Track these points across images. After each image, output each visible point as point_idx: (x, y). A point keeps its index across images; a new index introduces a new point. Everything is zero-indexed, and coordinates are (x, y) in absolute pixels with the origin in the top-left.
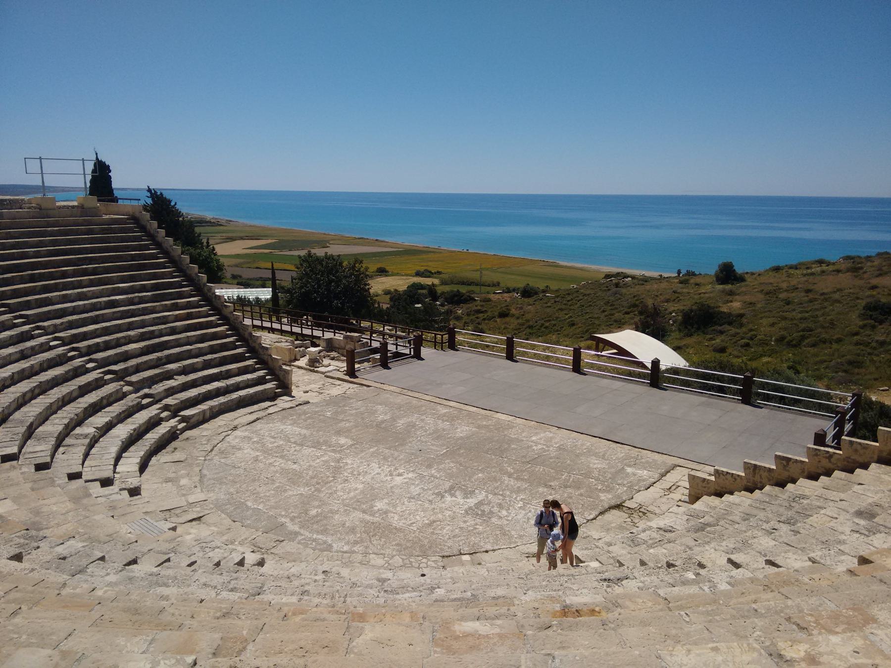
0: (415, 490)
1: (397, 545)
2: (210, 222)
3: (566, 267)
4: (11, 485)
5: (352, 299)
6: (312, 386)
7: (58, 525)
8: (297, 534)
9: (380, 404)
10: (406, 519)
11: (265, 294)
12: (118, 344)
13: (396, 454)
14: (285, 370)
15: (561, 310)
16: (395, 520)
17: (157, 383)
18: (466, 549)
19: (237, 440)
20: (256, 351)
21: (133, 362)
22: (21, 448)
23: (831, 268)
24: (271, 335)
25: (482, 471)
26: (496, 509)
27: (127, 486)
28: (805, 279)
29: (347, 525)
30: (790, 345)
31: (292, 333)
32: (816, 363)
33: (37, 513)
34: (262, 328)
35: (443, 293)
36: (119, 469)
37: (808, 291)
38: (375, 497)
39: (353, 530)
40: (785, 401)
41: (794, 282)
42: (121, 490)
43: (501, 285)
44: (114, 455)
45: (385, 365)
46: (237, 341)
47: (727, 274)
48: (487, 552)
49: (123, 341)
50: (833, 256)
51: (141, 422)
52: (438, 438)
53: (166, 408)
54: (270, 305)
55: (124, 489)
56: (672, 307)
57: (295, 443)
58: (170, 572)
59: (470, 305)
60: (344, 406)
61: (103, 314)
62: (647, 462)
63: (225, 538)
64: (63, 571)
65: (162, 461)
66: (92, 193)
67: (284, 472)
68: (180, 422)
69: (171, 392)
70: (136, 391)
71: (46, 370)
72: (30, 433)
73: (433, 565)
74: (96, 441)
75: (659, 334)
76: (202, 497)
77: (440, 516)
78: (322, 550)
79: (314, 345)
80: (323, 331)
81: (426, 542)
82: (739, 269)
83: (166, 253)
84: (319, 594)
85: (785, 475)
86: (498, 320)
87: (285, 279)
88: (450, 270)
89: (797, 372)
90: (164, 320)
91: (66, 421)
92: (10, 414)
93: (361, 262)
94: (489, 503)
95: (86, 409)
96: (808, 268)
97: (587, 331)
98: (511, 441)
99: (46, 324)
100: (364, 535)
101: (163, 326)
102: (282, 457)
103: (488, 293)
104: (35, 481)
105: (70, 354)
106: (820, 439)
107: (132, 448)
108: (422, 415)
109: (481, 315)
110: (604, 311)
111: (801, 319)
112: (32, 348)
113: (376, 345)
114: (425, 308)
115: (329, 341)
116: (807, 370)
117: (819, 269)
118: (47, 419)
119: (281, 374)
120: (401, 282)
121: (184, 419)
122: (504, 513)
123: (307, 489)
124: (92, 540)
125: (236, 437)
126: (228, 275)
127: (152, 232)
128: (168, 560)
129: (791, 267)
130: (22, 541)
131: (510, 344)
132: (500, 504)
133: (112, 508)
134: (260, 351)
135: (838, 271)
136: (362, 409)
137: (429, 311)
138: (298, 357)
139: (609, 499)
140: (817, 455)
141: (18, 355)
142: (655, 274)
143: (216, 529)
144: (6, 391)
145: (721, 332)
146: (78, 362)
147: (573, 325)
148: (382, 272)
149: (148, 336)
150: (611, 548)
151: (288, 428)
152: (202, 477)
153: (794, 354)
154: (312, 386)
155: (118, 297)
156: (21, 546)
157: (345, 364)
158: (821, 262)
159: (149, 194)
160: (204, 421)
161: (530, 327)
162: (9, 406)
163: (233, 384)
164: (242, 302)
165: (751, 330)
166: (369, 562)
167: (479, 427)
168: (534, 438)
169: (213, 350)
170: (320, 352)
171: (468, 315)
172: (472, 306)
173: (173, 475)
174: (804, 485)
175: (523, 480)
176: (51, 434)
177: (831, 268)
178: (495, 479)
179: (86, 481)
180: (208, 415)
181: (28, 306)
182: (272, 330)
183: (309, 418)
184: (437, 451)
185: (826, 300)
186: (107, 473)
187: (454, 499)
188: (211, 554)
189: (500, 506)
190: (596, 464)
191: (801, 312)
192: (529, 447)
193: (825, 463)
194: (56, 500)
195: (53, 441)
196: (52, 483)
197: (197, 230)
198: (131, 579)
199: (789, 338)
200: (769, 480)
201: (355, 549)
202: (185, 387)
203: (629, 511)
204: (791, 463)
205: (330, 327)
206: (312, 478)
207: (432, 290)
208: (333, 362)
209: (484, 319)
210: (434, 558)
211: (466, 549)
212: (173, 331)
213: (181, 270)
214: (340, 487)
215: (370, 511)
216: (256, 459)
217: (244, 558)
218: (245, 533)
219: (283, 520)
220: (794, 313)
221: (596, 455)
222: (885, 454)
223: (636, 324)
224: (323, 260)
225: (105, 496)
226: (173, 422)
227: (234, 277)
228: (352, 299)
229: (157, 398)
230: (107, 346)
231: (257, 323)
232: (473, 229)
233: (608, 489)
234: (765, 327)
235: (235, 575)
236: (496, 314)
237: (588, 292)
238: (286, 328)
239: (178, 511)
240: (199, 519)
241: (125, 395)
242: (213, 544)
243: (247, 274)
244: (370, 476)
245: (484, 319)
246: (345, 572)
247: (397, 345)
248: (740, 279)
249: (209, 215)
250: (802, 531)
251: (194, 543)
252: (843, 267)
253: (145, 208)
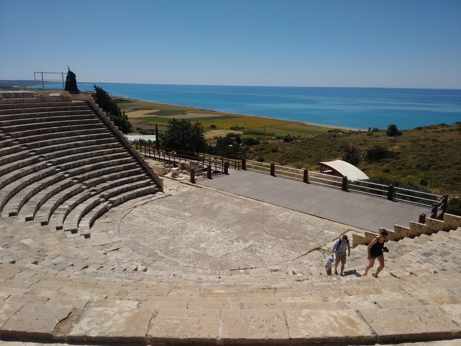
0: (220, 239)
1: (209, 264)
2: (126, 101)
3: (310, 126)
4: (31, 232)
5: (195, 143)
6: (173, 187)
7: (52, 250)
8: (163, 257)
9: (206, 197)
10: (215, 252)
11: (153, 138)
12: (80, 165)
13: (212, 221)
14: (161, 180)
15: (305, 149)
16: (209, 252)
17: (98, 184)
18: (242, 267)
19: (136, 213)
20: (146, 169)
21: (87, 174)
22: (35, 214)
23: (448, 128)
24: (154, 161)
25: (253, 230)
26: (258, 249)
27: (84, 234)
28: (433, 134)
29: (187, 254)
30: (423, 169)
31: (164, 160)
32: (436, 179)
33: (43, 245)
34: (150, 157)
35: (244, 139)
36: (80, 225)
37: (435, 141)
38: (200, 242)
39: (189, 257)
40: (413, 199)
41: (428, 136)
42: (81, 235)
43: (276, 135)
44: (78, 219)
45: (210, 177)
46: (137, 164)
47: (393, 131)
48: (252, 268)
49: (82, 163)
50: (450, 122)
51: (91, 203)
52: (233, 214)
53: (102, 196)
54: (155, 145)
55: (83, 235)
56: (362, 148)
57: (164, 215)
58: (103, 272)
59: (258, 146)
60: (188, 197)
61: (72, 151)
62: (335, 228)
63: (129, 258)
64: (55, 269)
65: (100, 222)
66: (66, 89)
67: (158, 228)
68: (109, 203)
69: (105, 189)
70: (88, 188)
71: (45, 177)
72: (38, 208)
73: (226, 273)
74: (69, 212)
75: (354, 162)
76: (119, 239)
77: (231, 251)
78: (174, 266)
79: (175, 166)
80: (180, 159)
81: (223, 263)
82: (399, 129)
83: (103, 120)
84: (167, 282)
85: (399, 235)
86: (272, 154)
87: (163, 130)
88: (248, 127)
89: (426, 184)
90: (102, 154)
91: (55, 202)
92: (29, 198)
93: (200, 124)
94: (255, 246)
95: (64, 196)
96: (436, 128)
97: (317, 160)
98: (269, 216)
99: (45, 155)
100: (194, 259)
101: (101, 157)
102: (157, 221)
103: (268, 139)
104: (41, 230)
105: (57, 170)
106: (422, 219)
107: (86, 216)
108: (226, 202)
109: (262, 151)
110: (327, 150)
111: (429, 155)
112: (39, 167)
113: (205, 167)
114: (234, 147)
115: (183, 164)
116: (431, 182)
117: (441, 129)
118: (46, 201)
119: (158, 181)
120: (223, 133)
121: (111, 202)
122: (262, 250)
123: (168, 237)
124: (68, 258)
125: (136, 211)
126: (135, 128)
127: (96, 109)
128: (102, 267)
129: (427, 128)
130: (37, 256)
131: (273, 167)
132: (261, 246)
133: (77, 243)
134: (148, 169)
135: (452, 130)
136: (197, 199)
137: (236, 149)
138: (167, 172)
139: (314, 245)
140: (414, 226)
141: (32, 170)
142: (356, 130)
143: (125, 254)
144: (27, 187)
145: (387, 162)
146: (60, 174)
147: (310, 157)
148: (213, 127)
149: (94, 161)
150: (310, 268)
151: (161, 207)
152: (119, 230)
153: (425, 174)
154: (173, 187)
155: (79, 142)
156: (37, 258)
157: (190, 176)
158: (443, 125)
159: (95, 89)
160: (121, 203)
161: (288, 157)
162: (29, 194)
163: (135, 186)
164: (142, 142)
165: (403, 161)
166: (196, 271)
167: (254, 209)
168: (280, 215)
169: (125, 168)
170: (178, 170)
171: (256, 151)
172: (258, 146)
173: (105, 229)
174: (407, 241)
175: (273, 235)
176: (48, 208)
177: (448, 128)
178: (259, 234)
179: (65, 231)
180: (122, 200)
181: (37, 146)
182: (155, 159)
183: (171, 203)
184: (232, 220)
185: (444, 146)
186: (75, 227)
187: (238, 243)
188: (122, 266)
189: (261, 247)
190: (310, 228)
191: (430, 152)
192: (277, 219)
193: (418, 230)
194: (51, 239)
195: (49, 212)
196: (49, 231)
197: (119, 105)
198: (85, 274)
199: (423, 165)
200: (391, 238)
201: (190, 265)
202: (112, 187)
203: (323, 251)
205: (183, 157)
206: (171, 232)
207: (237, 137)
208: (184, 175)
209: (264, 153)
210: (226, 271)
211: (242, 267)
212: (106, 159)
213: (110, 129)
214: (184, 236)
215: (197, 248)
216: (145, 222)
217: (137, 268)
218: (140, 257)
219: (157, 251)
220: (426, 152)
221: (310, 224)
222: (447, 226)
223: (343, 157)
224: (181, 123)
225: (73, 238)
226: (106, 203)
227: (138, 129)
228: (195, 143)
229: (98, 192)
230: (74, 166)
231: (148, 155)
232: (263, 105)
233: (314, 241)
234: (410, 159)
235: (132, 274)
236: (271, 150)
237: (318, 140)
238: (162, 157)
239: (108, 246)
240: (117, 249)
241: (83, 190)
242: (123, 261)
243: (145, 128)
244: (199, 232)
245: (264, 153)
246: (184, 275)
247: (216, 167)
248: (400, 134)
249: (126, 97)
250: (397, 262)
251: (115, 260)
252: (454, 128)
253: (93, 95)
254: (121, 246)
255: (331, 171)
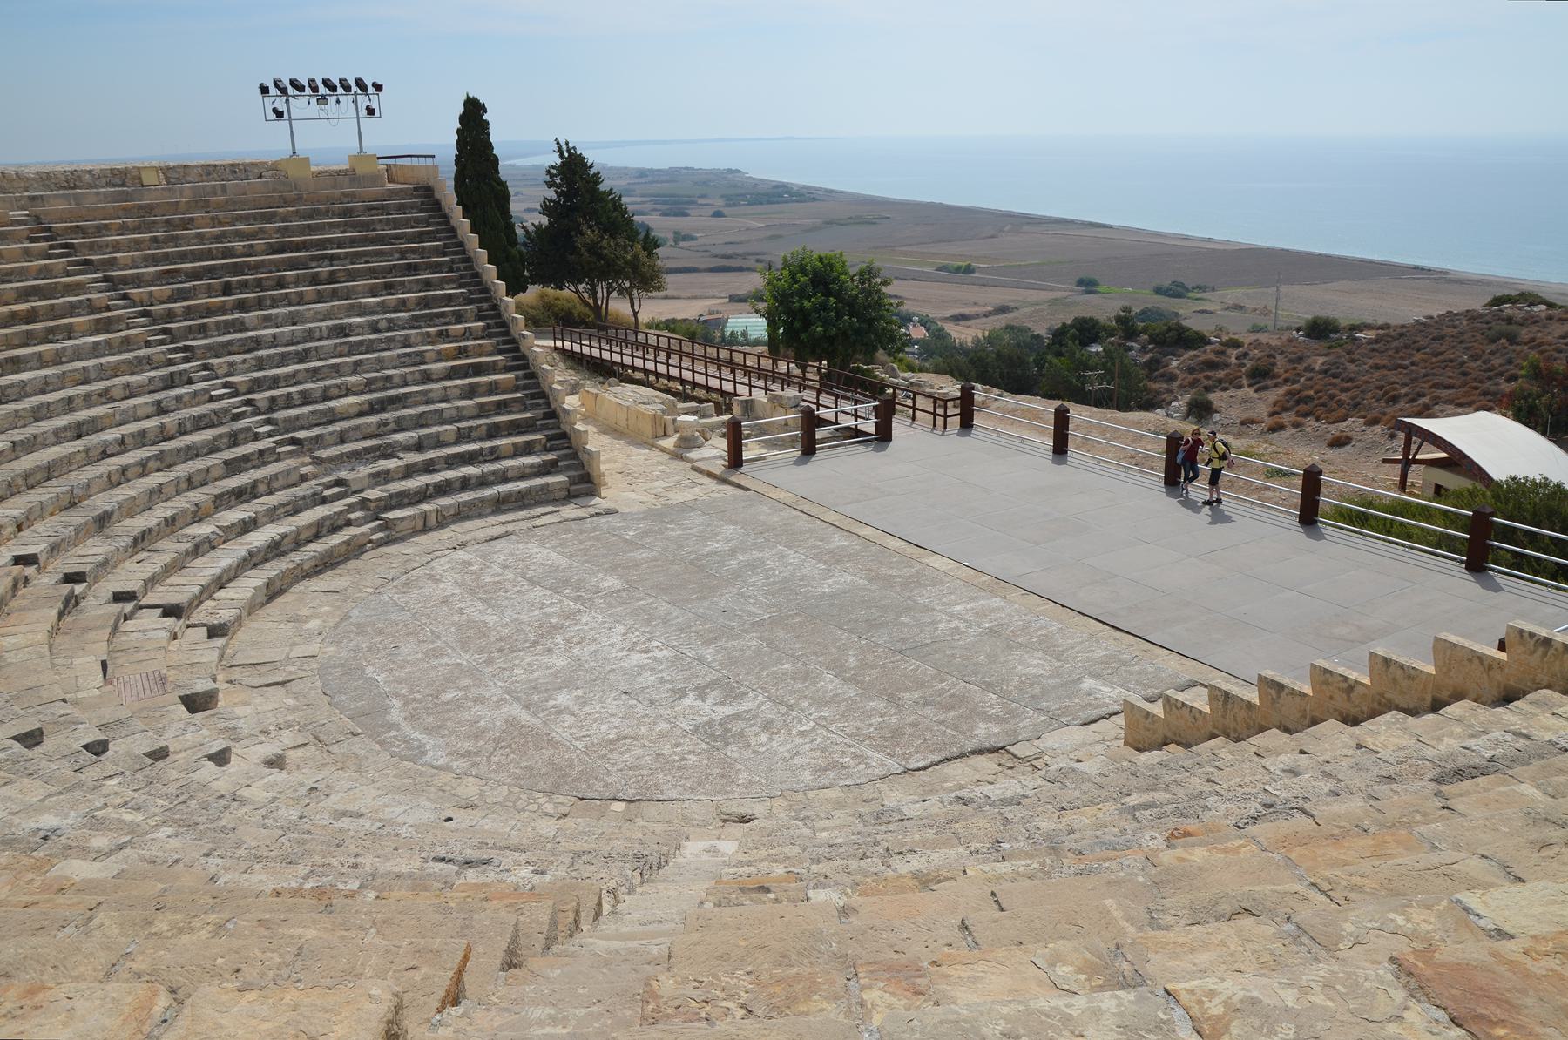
49: (335, 391)
140: (1327, 683)
204: (1283, 695)
223: (1520, 409)
229: (354, 488)
254: (302, 674)
255: (1444, 455)
